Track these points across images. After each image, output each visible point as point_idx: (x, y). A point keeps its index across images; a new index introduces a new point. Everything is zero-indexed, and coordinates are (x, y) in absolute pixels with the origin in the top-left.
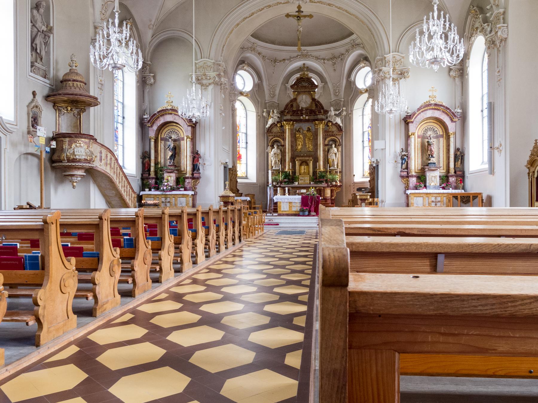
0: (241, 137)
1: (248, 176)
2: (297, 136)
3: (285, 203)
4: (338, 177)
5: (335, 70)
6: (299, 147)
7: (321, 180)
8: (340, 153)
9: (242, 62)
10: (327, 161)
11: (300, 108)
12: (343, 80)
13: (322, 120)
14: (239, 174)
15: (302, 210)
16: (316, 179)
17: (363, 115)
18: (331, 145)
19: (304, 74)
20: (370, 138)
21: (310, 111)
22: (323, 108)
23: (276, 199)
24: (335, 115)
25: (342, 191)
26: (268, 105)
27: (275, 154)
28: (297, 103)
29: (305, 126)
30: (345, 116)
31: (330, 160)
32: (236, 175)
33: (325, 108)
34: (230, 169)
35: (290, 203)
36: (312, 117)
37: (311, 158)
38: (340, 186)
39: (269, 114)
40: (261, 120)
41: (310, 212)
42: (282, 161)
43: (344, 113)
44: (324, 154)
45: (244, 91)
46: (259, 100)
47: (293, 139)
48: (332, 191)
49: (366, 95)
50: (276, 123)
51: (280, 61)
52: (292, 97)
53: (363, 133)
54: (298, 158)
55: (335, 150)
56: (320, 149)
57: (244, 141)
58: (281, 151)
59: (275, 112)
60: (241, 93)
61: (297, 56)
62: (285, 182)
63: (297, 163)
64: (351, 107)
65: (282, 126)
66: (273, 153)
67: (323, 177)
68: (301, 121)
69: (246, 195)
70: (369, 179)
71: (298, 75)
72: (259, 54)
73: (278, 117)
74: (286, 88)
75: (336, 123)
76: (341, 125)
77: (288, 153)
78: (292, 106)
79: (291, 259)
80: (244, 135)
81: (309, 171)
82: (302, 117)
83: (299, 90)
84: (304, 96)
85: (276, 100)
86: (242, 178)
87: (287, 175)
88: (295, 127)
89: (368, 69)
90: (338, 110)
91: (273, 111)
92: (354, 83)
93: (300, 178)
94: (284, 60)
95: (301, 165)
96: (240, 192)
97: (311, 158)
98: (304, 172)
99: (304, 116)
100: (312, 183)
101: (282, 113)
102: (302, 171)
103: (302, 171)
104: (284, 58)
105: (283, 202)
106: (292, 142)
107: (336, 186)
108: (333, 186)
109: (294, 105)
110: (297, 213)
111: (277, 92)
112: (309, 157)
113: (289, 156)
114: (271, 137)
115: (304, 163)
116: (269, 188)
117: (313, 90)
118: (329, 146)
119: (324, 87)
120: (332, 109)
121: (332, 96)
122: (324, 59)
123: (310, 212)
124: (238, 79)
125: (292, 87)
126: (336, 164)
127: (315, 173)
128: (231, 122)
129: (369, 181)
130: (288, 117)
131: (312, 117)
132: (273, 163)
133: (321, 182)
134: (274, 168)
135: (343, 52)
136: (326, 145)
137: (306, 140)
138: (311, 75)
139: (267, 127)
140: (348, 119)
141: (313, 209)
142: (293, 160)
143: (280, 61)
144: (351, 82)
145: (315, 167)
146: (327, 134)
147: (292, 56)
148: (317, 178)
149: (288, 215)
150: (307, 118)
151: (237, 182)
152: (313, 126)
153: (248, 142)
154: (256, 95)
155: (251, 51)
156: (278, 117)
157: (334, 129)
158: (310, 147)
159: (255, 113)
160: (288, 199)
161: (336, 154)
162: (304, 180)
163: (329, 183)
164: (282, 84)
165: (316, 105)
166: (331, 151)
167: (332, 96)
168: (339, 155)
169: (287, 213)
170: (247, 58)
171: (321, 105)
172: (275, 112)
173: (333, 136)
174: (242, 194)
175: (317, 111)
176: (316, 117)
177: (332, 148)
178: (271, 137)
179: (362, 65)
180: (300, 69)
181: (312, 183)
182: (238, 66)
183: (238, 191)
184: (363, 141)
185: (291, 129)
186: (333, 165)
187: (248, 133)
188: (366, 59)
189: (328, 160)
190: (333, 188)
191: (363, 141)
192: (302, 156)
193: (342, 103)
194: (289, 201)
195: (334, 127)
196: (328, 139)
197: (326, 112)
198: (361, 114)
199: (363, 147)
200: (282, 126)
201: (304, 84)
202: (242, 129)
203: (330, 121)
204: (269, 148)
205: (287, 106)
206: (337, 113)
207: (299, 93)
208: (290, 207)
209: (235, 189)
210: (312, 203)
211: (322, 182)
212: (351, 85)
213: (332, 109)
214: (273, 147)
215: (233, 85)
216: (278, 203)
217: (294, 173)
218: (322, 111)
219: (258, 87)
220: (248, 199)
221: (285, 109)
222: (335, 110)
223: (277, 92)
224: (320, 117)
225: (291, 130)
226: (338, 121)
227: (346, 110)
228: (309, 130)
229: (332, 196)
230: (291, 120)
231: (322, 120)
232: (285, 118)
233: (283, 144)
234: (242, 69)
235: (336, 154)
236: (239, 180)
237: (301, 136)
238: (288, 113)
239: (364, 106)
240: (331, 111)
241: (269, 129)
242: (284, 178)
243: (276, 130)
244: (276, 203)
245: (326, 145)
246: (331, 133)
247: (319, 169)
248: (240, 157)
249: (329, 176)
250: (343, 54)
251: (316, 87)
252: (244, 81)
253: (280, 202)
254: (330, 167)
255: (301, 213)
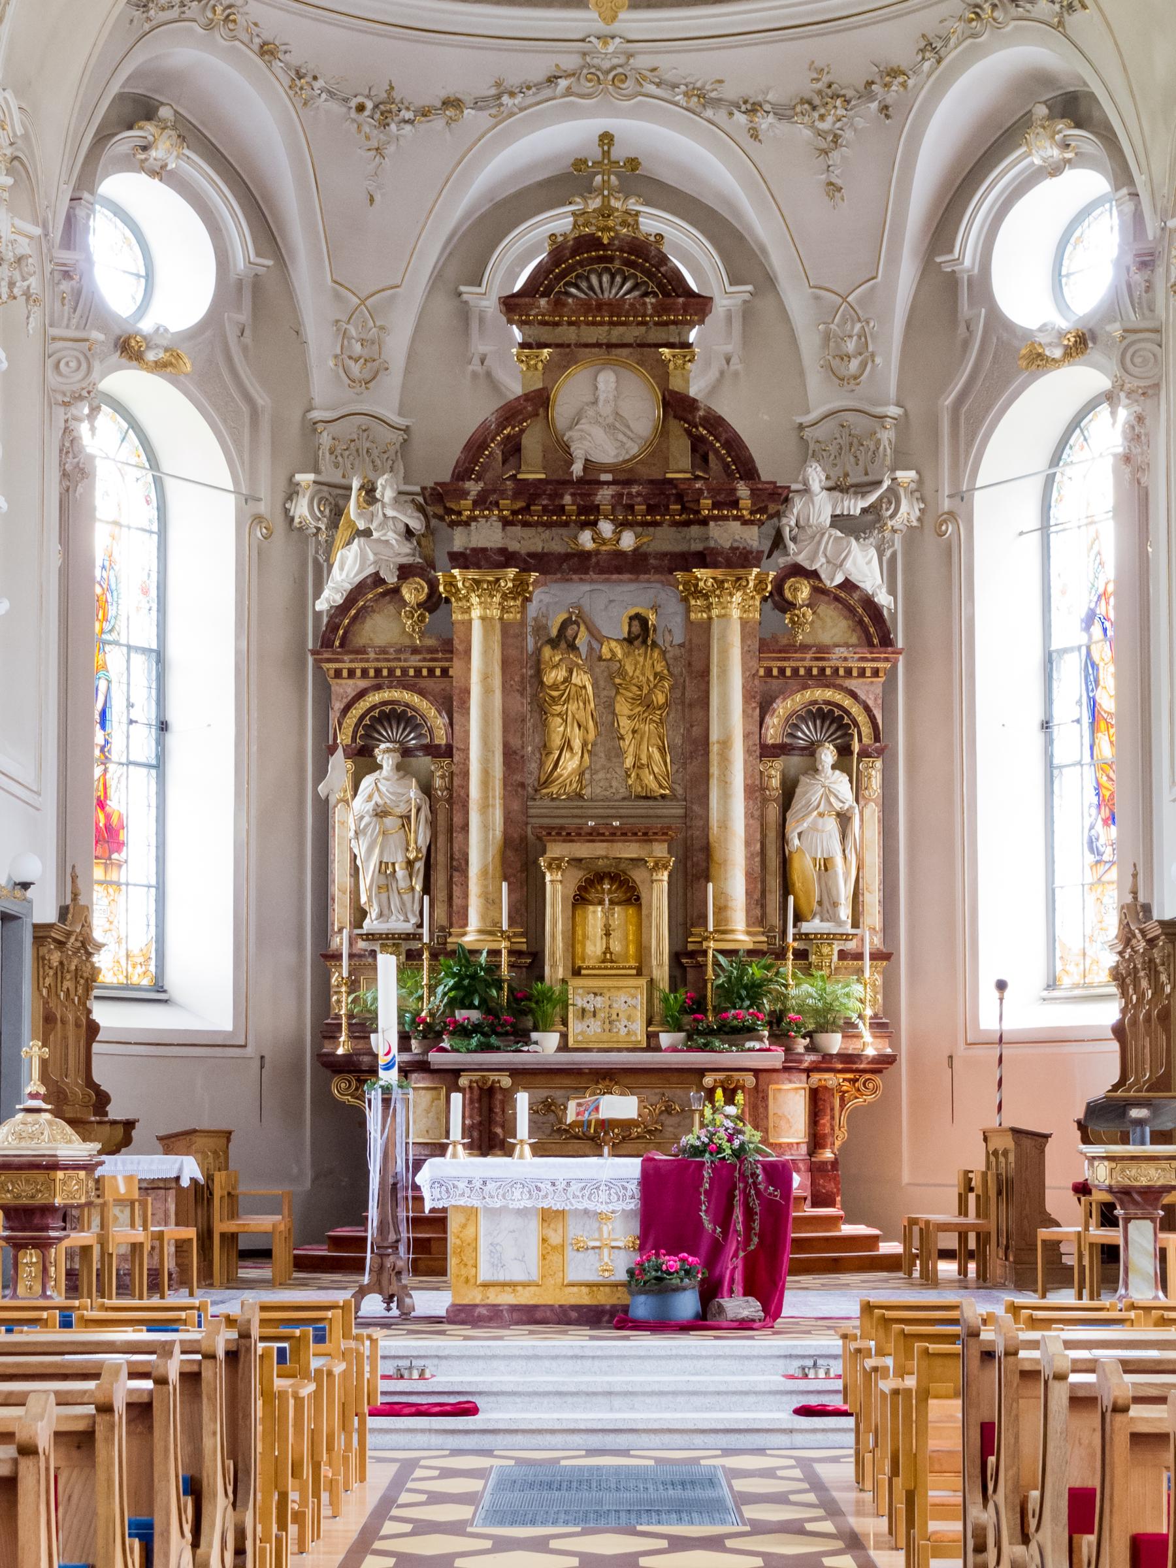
0: (123, 680)
1: (174, 980)
2: (553, 676)
3: (508, 1222)
4: (857, 996)
5: (833, 188)
6: (570, 764)
7: (741, 1014)
8: (873, 812)
9: (137, 109)
10: (776, 870)
11: (577, 469)
12: (894, 261)
13: (741, 559)
14: (109, 966)
15: (658, 1285)
16: (697, 1006)
17: (1045, 528)
18: (811, 750)
19: (605, 212)
20: (1107, 702)
21: (655, 497)
22: (749, 471)
23: (436, 1183)
24: (838, 521)
25: (890, 1101)
26: (325, 440)
27: (381, 813)
28: (548, 423)
29: (611, 606)
30: (913, 534)
31: (803, 867)
32: (87, 980)
33: (766, 473)
34: (41, 933)
35: (548, 1216)
36: (665, 540)
37: (660, 850)
38: (885, 1062)
39: (337, 513)
40: (282, 547)
41: (710, 1292)
42: (439, 868)
43: (907, 511)
44: (757, 816)
45: (146, 326)
46: (262, 400)
47: (522, 705)
48: (816, 1099)
49: (1086, 378)
50: (391, 579)
51: (425, 113)
52: (515, 387)
53: (1049, 661)
54: (556, 850)
55: (841, 784)
56: (725, 783)
57: (145, 711)
58: (426, 789)
59: (386, 489)
60: (129, 348)
61: (552, 80)
62: (464, 1032)
63: (556, 889)
64: (956, 466)
65: (434, 602)
66: (370, 810)
67: (755, 991)
68: (579, 564)
69: (171, 1143)
70: (1109, 1013)
71: (559, 222)
72: (267, 51)
73: (409, 533)
74: (464, 314)
75: (848, 585)
76: (883, 599)
77: (485, 807)
78: (513, 449)
79: (408, 1528)
80: (142, 667)
81: (642, 952)
82: (586, 540)
83: (569, 334)
84: (607, 380)
85: (386, 401)
86: (125, 996)
87: (472, 981)
88: (533, 609)
89: (1087, 183)
90: (861, 489)
91: (369, 490)
92: (981, 284)
93: (578, 999)
94: (452, 103)
95: (580, 900)
96: (115, 1112)
97: (660, 850)
98: (608, 957)
99: (606, 528)
100: (665, 1039)
101: (438, 503)
102: (594, 948)
103: (594, 948)
104: (452, 89)
105: (493, 1213)
106: (510, 722)
107: (849, 1059)
108: (826, 1063)
109: (532, 442)
110: (604, 1298)
111: (397, 346)
112: (646, 836)
113: (486, 827)
114: (346, 688)
115: (613, 884)
116: (376, 1096)
117: (672, 334)
118: (795, 761)
119: (748, 313)
120: (816, 476)
121: (815, 380)
122: (753, 109)
123: (710, 1292)
124: (104, 238)
125: (512, 305)
126: (844, 892)
127: (686, 961)
128: (55, 561)
129: (1119, 1031)
130: (487, 534)
131: (665, 540)
132: (366, 881)
133: (738, 1033)
134: (369, 925)
135: (903, 56)
136: (768, 751)
137: (623, 707)
138: (654, 222)
139: (322, 605)
140: (939, 552)
141: (733, 1265)
142: (521, 861)
143: (425, 113)
144: (951, 282)
145: (689, 914)
146: (778, 662)
147: (512, 81)
148: (710, 1001)
149: (532, 1316)
150: (628, 541)
151: (93, 1029)
152: (673, 606)
153: (173, 717)
154: (245, 348)
155: (209, 26)
156: (409, 533)
157: (830, 628)
158: (648, 759)
159: (230, 501)
160: (533, 1187)
161: (844, 819)
162: (609, 1015)
163: (801, 1044)
164: (437, 278)
165: (700, 451)
166: (811, 793)
167: (815, 380)
168: (867, 827)
169: (525, 1297)
170: (172, 79)
171: (734, 444)
172: (386, 489)
173: (823, 679)
174: (129, 1125)
175: (702, 492)
176: (692, 539)
177: (813, 769)
178: (346, 688)
179: (1041, 150)
180: (571, 180)
181: (665, 1039)
182: (102, 138)
183: (102, 1100)
184: (1046, 725)
185: (505, 627)
186: (828, 906)
187: (174, 652)
188: (1074, 107)
189: (785, 863)
190: (831, 1080)
191: (1046, 725)
192: (593, 835)
193: (887, 436)
194: (543, 1206)
195: (828, 611)
196: (783, 708)
197: (773, 499)
198: (1032, 520)
199: (1050, 769)
200: (434, 602)
201: (609, 283)
202: (130, 619)
203: (797, 571)
204: (340, 766)
205: (476, 447)
206: (855, 506)
207: (568, 354)
208: (548, 1249)
209: (74, 1084)
210: (724, 1219)
211: (750, 1031)
212: (952, 300)
213: (816, 476)
214: (363, 757)
215: (69, 282)
216: (453, 1225)
217: (531, 960)
218: (743, 490)
219: (256, 303)
220: (189, 1168)
221: (463, 473)
222: (837, 488)
223: (397, 346)
224: (728, 534)
225: (509, 633)
226: (864, 566)
227: (919, 491)
228: (641, 633)
229: (816, 1141)
230: (507, 558)
231: (741, 559)
232: (460, 540)
233: (441, 738)
234: (137, 159)
235: (844, 819)
236: (104, 1015)
237: (581, 678)
238: (481, 501)
239: (1056, 459)
240: (806, 491)
241: (333, 627)
242: (453, 1004)
243: (383, 629)
244: (439, 1221)
245: (768, 751)
246: (806, 661)
247: (722, 930)
248: (110, 837)
249: (802, 991)
250: (894, 73)
251: (699, 306)
252: (155, 251)
253: (471, 1213)
254: (798, 918)
255: (642, 1307)
